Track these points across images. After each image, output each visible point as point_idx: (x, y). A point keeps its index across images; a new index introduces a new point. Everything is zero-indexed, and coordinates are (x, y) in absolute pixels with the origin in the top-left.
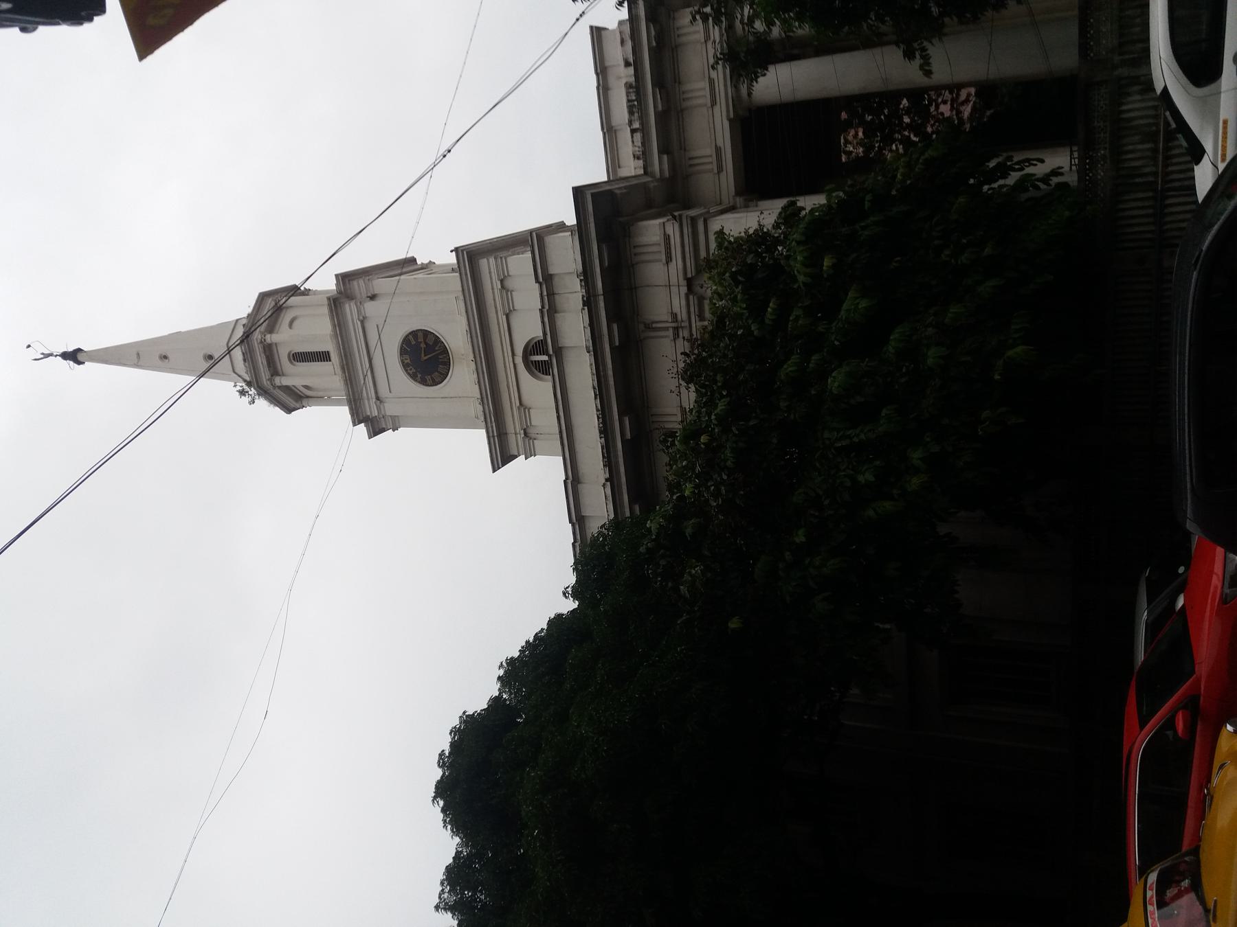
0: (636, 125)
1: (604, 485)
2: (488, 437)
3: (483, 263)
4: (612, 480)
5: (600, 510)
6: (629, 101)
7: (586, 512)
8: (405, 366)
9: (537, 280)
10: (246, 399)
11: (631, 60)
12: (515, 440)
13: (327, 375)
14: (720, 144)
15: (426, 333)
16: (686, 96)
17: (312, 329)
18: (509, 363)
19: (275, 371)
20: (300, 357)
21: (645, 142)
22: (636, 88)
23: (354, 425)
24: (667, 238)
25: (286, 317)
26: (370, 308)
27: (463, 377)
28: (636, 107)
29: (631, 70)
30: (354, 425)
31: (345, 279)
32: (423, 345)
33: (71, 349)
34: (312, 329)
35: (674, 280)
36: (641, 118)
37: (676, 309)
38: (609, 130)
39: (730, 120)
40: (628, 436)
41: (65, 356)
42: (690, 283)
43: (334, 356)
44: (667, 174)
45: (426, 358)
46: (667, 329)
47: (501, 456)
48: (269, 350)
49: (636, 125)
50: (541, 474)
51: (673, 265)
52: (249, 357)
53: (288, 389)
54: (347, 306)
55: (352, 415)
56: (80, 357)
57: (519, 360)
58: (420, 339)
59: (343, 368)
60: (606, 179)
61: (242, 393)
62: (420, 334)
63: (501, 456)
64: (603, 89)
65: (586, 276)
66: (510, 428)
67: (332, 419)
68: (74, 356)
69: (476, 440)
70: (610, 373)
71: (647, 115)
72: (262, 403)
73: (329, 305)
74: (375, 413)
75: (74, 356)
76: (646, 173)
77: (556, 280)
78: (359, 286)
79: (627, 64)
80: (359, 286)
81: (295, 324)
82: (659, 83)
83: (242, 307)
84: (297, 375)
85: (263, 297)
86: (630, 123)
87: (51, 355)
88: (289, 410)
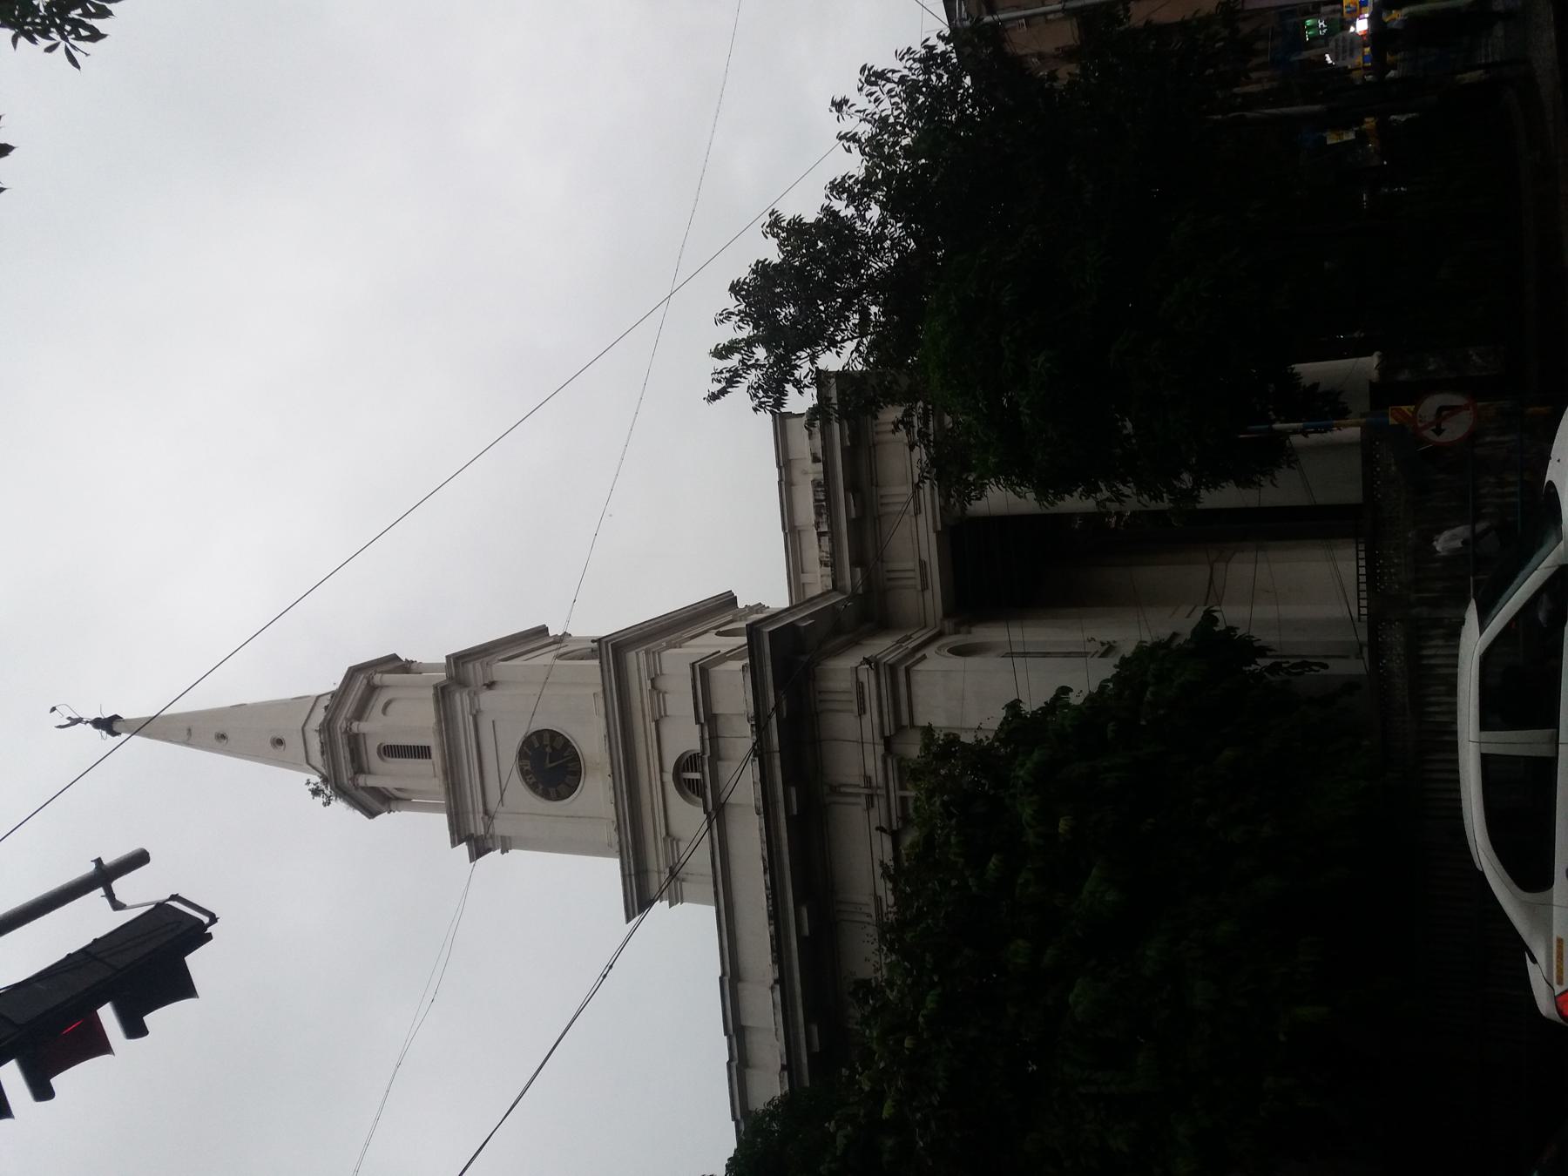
0: (824, 528)
1: (772, 988)
2: (623, 876)
3: (631, 656)
4: (782, 981)
5: (769, 1087)
6: (816, 500)
7: (748, 1021)
8: (524, 774)
9: (698, 721)
10: (320, 800)
11: (820, 456)
12: (655, 881)
13: (425, 775)
14: (925, 557)
15: (554, 735)
16: (885, 501)
17: (409, 716)
18: (656, 783)
19: (359, 768)
20: (390, 751)
21: (835, 552)
22: (824, 488)
23: (454, 844)
24: (860, 686)
25: (380, 700)
26: (487, 699)
27: (596, 792)
28: (825, 507)
29: (820, 466)
30: (454, 844)
31: (458, 660)
32: (548, 750)
33: (107, 715)
34: (409, 716)
35: (868, 736)
36: (830, 516)
37: (871, 772)
38: (791, 530)
39: (938, 533)
40: (806, 931)
41: (98, 723)
42: (888, 742)
43: (436, 753)
44: (860, 591)
45: (550, 765)
46: (858, 795)
47: (638, 900)
48: (355, 742)
49: (824, 528)
50: (686, 931)
51: (866, 718)
52: (328, 748)
53: (375, 791)
54: (457, 696)
55: (452, 834)
56: (116, 726)
57: (669, 777)
58: (546, 741)
59: (445, 773)
60: (787, 605)
61: (316, 792)
62: (547, 736)
63: (638, 900)
64: (786, 485)
65: (759, 724)
66: (652, 864)
67: (421, 830)
68: (108, 725)
69: (606, 873)
70: (785, 849)
71: (838, 525)
72: (339, 806)
73: (436, 695)
74: (481, 831)
75: (108, 725)
76: (835, 587)
77: (721, 721)
78: (474, 670)
79: (815, 460)
80: (474, 670)
81: (390, 709)
82: (853, 486)
83: (331, 680)
84: (386, 774)
85: (354, 672)
86: (817, 525)
87: (79, 720)
88: (371, 814)
